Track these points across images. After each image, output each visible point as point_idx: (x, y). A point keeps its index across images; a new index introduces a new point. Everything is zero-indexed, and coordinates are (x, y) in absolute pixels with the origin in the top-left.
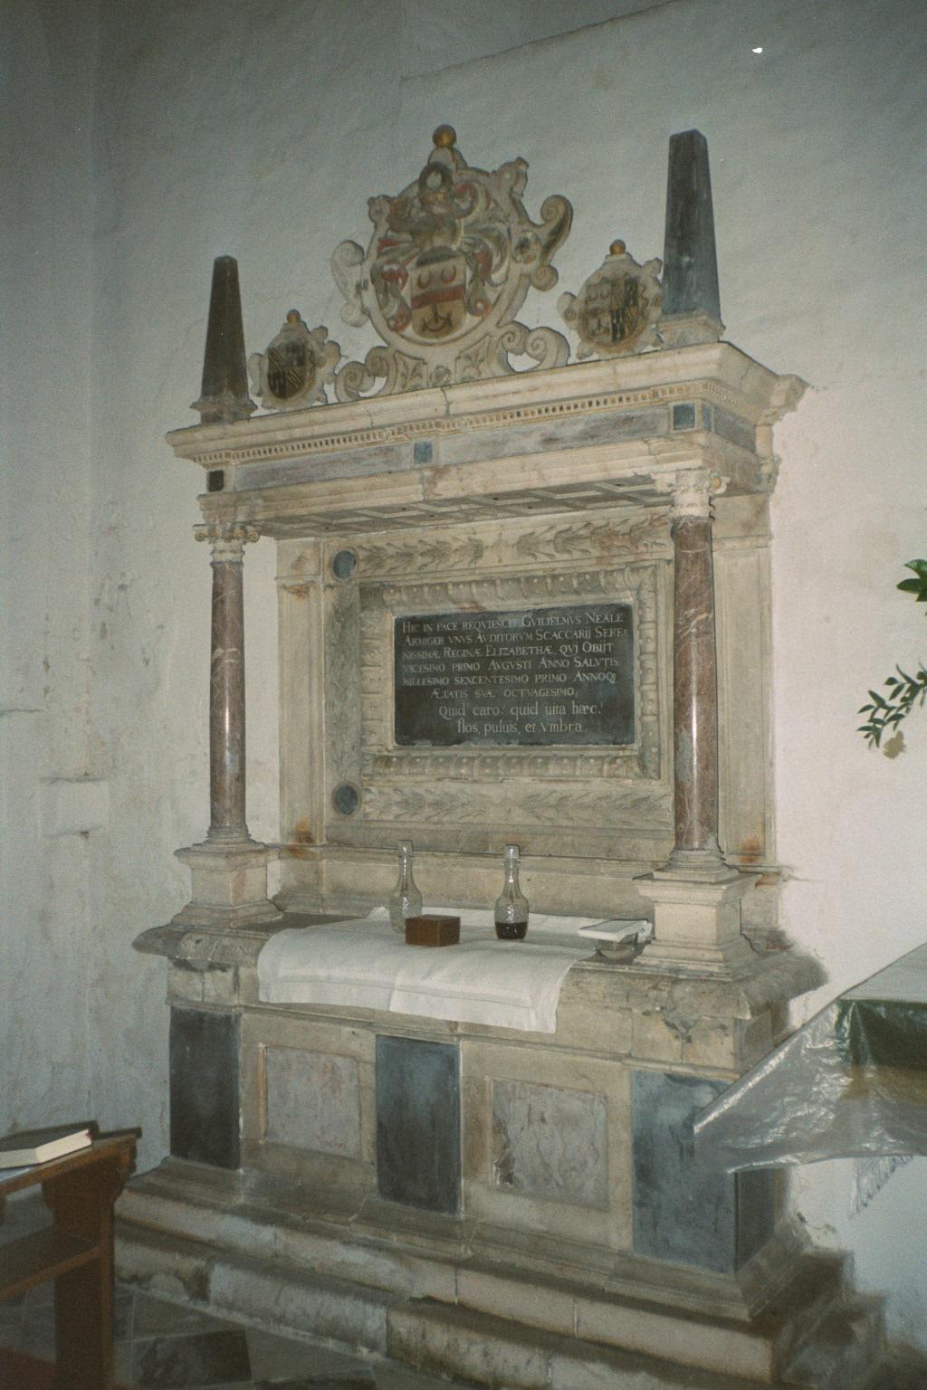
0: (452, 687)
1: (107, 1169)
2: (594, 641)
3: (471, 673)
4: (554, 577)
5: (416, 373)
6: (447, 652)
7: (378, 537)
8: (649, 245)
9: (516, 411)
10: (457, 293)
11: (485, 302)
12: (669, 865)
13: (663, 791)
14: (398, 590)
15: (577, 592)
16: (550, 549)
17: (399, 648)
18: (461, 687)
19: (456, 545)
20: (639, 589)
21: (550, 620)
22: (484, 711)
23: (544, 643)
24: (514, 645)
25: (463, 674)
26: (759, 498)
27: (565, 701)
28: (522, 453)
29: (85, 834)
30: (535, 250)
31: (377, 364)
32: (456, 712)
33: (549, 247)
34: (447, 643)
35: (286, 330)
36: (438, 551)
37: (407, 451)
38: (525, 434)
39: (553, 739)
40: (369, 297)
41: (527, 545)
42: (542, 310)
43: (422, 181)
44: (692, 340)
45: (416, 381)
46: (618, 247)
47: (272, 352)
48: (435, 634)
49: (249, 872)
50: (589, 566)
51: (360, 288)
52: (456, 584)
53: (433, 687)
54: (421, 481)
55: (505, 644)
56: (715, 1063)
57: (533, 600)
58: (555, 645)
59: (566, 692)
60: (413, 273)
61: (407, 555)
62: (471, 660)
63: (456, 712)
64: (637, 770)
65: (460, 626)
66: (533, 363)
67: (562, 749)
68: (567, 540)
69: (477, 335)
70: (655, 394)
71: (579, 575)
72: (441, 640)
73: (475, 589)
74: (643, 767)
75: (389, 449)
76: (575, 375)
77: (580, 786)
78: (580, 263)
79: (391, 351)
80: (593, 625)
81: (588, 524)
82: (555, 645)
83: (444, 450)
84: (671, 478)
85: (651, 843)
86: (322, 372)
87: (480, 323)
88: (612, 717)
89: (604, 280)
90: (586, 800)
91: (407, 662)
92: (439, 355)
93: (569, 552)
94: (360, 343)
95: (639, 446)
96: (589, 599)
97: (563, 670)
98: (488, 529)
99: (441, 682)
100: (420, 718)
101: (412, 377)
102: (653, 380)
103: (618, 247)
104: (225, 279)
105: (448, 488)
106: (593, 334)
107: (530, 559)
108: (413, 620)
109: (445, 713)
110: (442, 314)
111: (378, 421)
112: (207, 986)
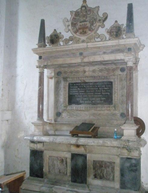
0: (79, 95)
1: (20, 180)
2: (106, 87)
3: (83, 93)
4: (99, 77)
5: (79, 41)
6: (78, 89)
7: (66, 69)
8: (123, 22)
9: (99, 48)
10: (87, 28)
11: (92, 29)
12: (125, 123)
13: (118, 112)
14: (70, 78)
15: (103, 79)
16: (98, 72)
17: (69, 88)
18: (81, 95)
19: (81, 71)
20: (115, 79)
22: (85, 99)
23: (96, 88)
24: (91, 88)
25: (81, 93)
26: (137, 64)
27: (100, 97)
28: (99, 55)
29: (7, 120)
30: (102, 21)
31: (71, 39)
33: (104, 21)
34: (78, 87)
35: (54, 32)
36: (77, 72)
37: (78, 54)
38: (100, 51)
39: (98, 104)
40: (70, 27)
41: (94, 71)
42: (101, 31)
43: (81, 8)
44: (131, 37)
45: (79, 42)
46: (116, 22)
47: (51, 36)
48: (76, 86)
49: (45, 126)
50: (105, 75)
51: (68, 26)
52: (81, 77)
54: (81, 59)
55: (89, 88)
56: (135, 155)
57: (95, 80)
58: (98, 88)
59: (101, 96)
60: (79, 24)
61: (71, 72)
62: (83, 90)
64: (114, 109)
65: (81, 84)
66: (100, 40)
67: (99, 105)
68: (101, 71)
69: (91, 34)
70: (125, 46)
71: (104, 76)
72: (77, 87)
73: (84, 78)
74: (115, 108)
75: (74, 53)
76: (108, 42)
77: (103, 112)
78: (109, 24)
79: (74, 37)
81: (105, 68)
82: (98, 88)
83: (85, 54)
84: (127, 59)
85: (116, 121)
86: (60, 40)
87: (91, 33)
88: (108, 99)
89: (114, 27)
90: (104, 114)
92: (83, 38)
93: (101, 72)
94: (67, 35)
95: (122, 54)
96: (105, 80)
97: (100, 92)
98: (87, 69)
99: (77, 94)
100: (71, 100)
101: (78, 41)
102: (125, 43)
103: (116, 22)
104: (43, 23)
105: (86, 60)
106: (112, 36)
107: (94, 74)
108: (72, 83)
109: (78, 99)
110: (84, 31)
111: (73, 48)
112: (38, 146)
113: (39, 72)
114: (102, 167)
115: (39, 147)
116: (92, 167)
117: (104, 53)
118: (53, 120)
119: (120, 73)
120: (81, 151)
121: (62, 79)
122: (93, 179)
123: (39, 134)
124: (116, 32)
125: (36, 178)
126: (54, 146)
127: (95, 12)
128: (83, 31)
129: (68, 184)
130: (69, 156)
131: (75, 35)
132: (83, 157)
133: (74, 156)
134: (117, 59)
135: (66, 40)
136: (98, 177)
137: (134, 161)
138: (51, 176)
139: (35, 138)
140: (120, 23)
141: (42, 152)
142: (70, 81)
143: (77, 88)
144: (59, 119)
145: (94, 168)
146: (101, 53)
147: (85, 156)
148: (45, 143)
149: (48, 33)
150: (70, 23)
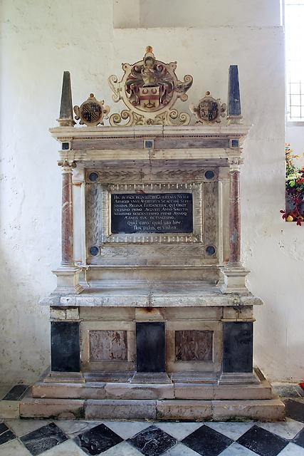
0: (132, 216)
6: (130, 205)
8: (223, 97)
21: (166, 197)
22: (144, 223)
24: (154, 204)
27: (171, 220)
31: (125, 115)
32: (134, 223)
40: (123, 93)
45: (141, 122)
47: (85, 106)
48: (126, 199)
51: (119, 90)
53: (125, 216)
54: (149, 153)
58: (168, 204)
63: (134, 223)
80: (180, 199)
82: (168, 204)
88: (185, 225)
91: (116, 208)
100: (118, 225)
109: (130, 223)
113: (63, 174)
114: (192, 340)
115: (72, 316)
116: (173, 342)
117: (191, 146)
118: (84, 262)
119: (206, 180)
120: (155, 316)
121: (99, 186)
122: (175, 361)
123: (69, 292)
124: (211, 111)
125: (67, 373)
126: (102, 311)
127: (170, 71)
128: (150, 104)
129: (131, 376)
130: (130, 327)
131: (133, 109)
132: (158, 328)
133: (140, 327)
134: (214, 157)
135: (115, 116)
136: (185, 357)
137: (245, 327)
138: (94, 366)
139: (65, 301)
140: (214, 96)
141: (76, 324)
142: (117, 190)
143: (128, 204)
144: (95, 259)
145: (177, 344)
146: (184, 145)
147: (161, 325)
148: (81, 309)
149: (78, 100)
150: (123, 85)
